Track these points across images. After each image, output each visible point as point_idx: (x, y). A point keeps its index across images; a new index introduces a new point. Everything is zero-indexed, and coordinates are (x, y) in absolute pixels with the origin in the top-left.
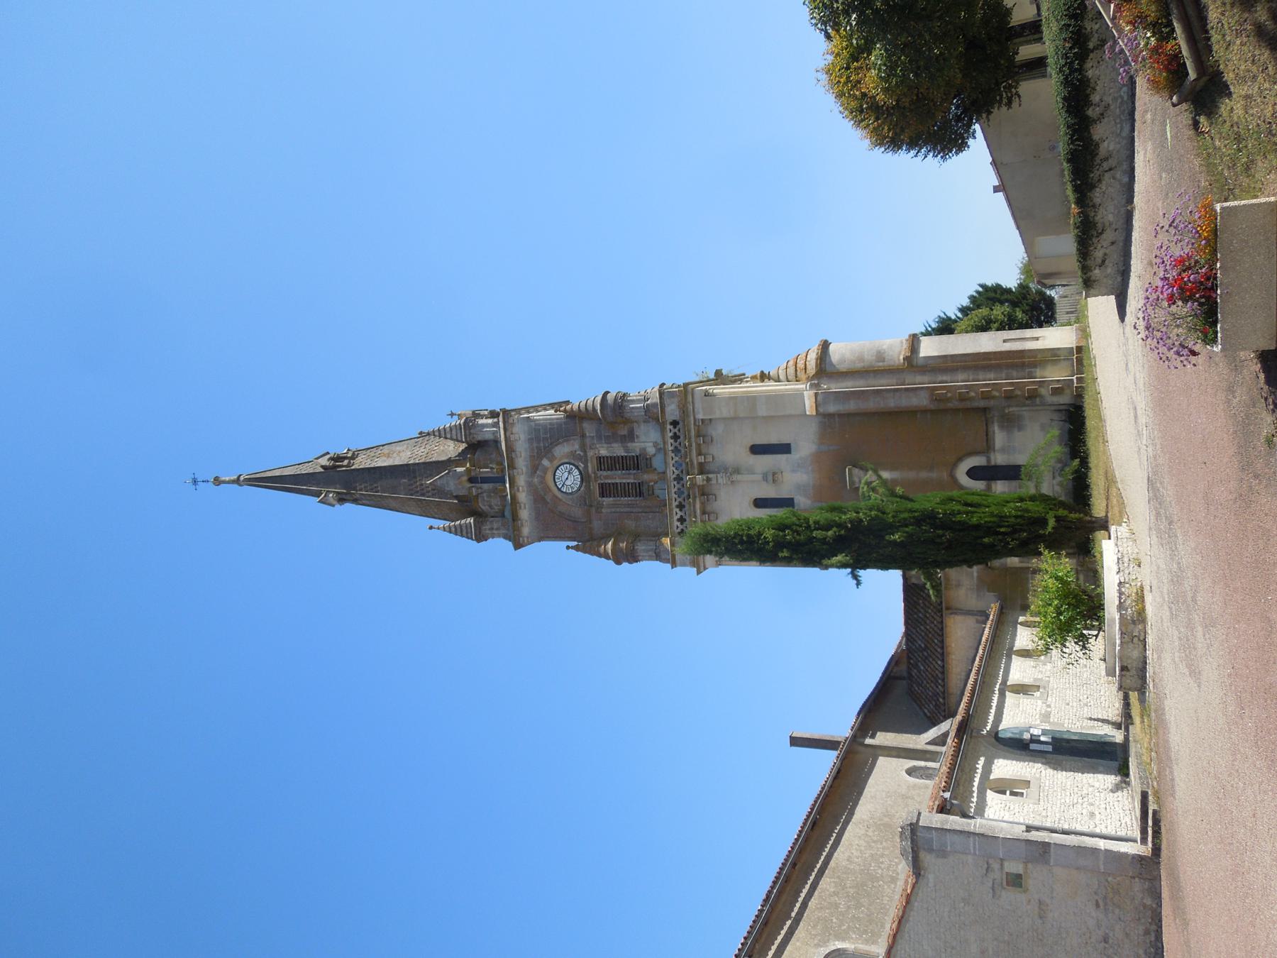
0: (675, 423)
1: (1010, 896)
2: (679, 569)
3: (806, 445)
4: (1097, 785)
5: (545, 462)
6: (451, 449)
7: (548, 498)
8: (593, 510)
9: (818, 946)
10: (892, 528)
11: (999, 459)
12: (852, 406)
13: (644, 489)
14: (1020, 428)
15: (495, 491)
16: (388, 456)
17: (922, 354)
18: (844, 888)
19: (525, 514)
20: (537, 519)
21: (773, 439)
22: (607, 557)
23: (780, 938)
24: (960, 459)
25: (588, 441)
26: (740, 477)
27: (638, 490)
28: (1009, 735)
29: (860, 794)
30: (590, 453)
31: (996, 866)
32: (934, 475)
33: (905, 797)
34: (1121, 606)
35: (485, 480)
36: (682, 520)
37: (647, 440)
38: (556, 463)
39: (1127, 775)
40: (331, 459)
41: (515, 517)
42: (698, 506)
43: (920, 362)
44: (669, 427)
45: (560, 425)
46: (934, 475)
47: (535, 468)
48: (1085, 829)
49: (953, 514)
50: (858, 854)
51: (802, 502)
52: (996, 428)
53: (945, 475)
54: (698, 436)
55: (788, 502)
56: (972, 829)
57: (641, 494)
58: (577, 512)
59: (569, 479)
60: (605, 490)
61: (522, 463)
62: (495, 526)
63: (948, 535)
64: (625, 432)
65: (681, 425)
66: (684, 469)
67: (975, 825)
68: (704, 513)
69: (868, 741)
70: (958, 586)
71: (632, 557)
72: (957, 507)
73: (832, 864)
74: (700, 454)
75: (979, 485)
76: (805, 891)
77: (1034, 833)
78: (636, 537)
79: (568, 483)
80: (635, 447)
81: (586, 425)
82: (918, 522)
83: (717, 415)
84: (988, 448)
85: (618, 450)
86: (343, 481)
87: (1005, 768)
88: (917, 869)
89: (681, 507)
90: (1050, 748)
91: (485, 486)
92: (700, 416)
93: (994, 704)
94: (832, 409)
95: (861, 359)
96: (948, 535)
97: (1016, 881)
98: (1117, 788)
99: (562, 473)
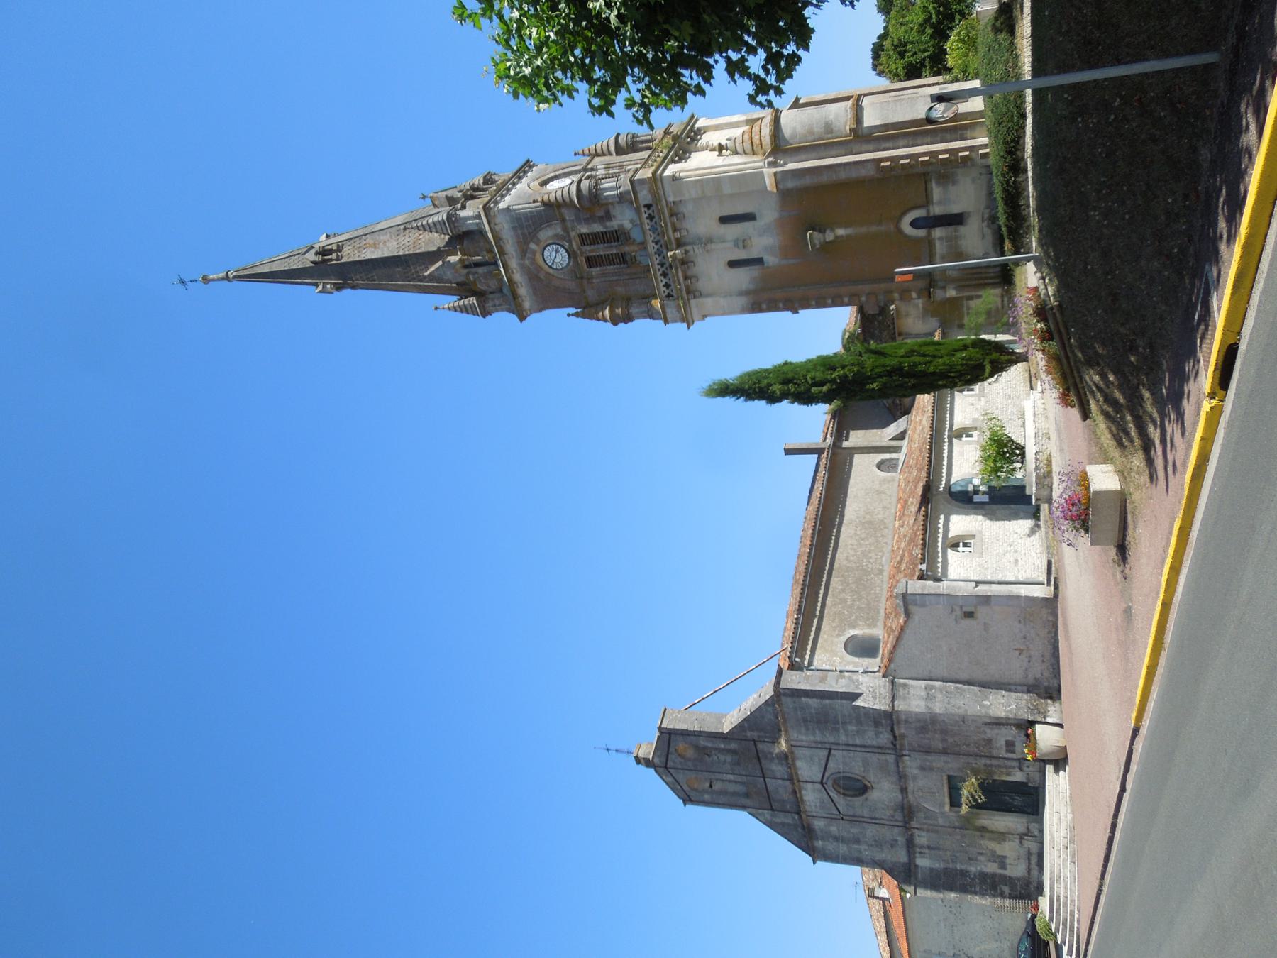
0: (648, 206)
1: (968, 622)
2: (671, 326)
3: (769, 214)
4: (1019, 531)
5: (533, 246)
6: (436, 241)
7: (542, 276)
8: (585, 281)
9: (839, 635)
10: (872, 379)
11: (937, 210)
12: (808, 181)
13: (628, 258)
14: (954, 183)
15: (490, 273)
16: (375, 246)
17: (866, 124)
18: (848, 584)
19: (523, 291)
20: (535, 294)
21: (740, 210)
22: (605, 321)
23: (812, 634)
24: (904, 213)
25: (569, 224)
26: (713, 246)
27: (622, 259)
28: (959, 488)
29: (846, 495)
30: (572, 234)
31: (958, 609)
32: (883, 228)
33: (879, 493)
34: (1037, 468)
35: (477, 265)
36: (667, 285)
37: (623, 219)
38: (543, 245)
39: (1038, 519)
40: (317, 254)
41: (515, 296)
42: (680, 274)
43: (865, 132)
44: (643, 209)
45: (539, 212)
46: (883, 228)
47: (523, 252)
48: (1012, 579)
49: (915, 365)
50: (852, 552)
51: (770, 260)
52: (934, 185)
53: (892, 227)
54: (671, 215)
55: (759, 261)
56: (941, 591)
57: (624, 262)
58: (571, 285)
59: (557, 257)
60: (591, 262)
61: (511, 247)
62: (497, 302)
63: (913, 381)
64: (601, 213)
65: (654, 207)
66: (662, 247)
67: (942, 587)
68: (686, 278)
69: (845, 444)
70: (907, 315)
71: (628, 318)
72: (918, 359)
73: (836, 565)
74: (675, 230)
75: (921, 233)
76: (822, 592)
77: (981, 587)
78: (628, 300)
79: (557, 260)
80: (614, 225)
81: (564, 211)
82: (890, 374)
83: (687, 196)
84: (927, 202)
85: (597, 228)
86: (331, 271)
87: (960, 523)
88: (908, 614)
89: (664, 275)
90: (986, 498)
91: (480, 270)
92: (671, 199)
93: (945, 455)
94: (790, 184)
95: (811, 132)
96: (913, 381)
97: (969, 615)
98: (1033, 532)
99: (550, 253)
